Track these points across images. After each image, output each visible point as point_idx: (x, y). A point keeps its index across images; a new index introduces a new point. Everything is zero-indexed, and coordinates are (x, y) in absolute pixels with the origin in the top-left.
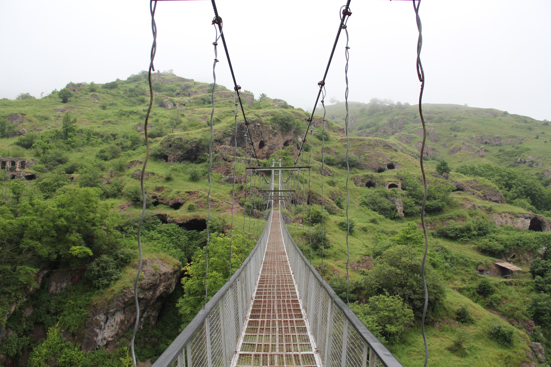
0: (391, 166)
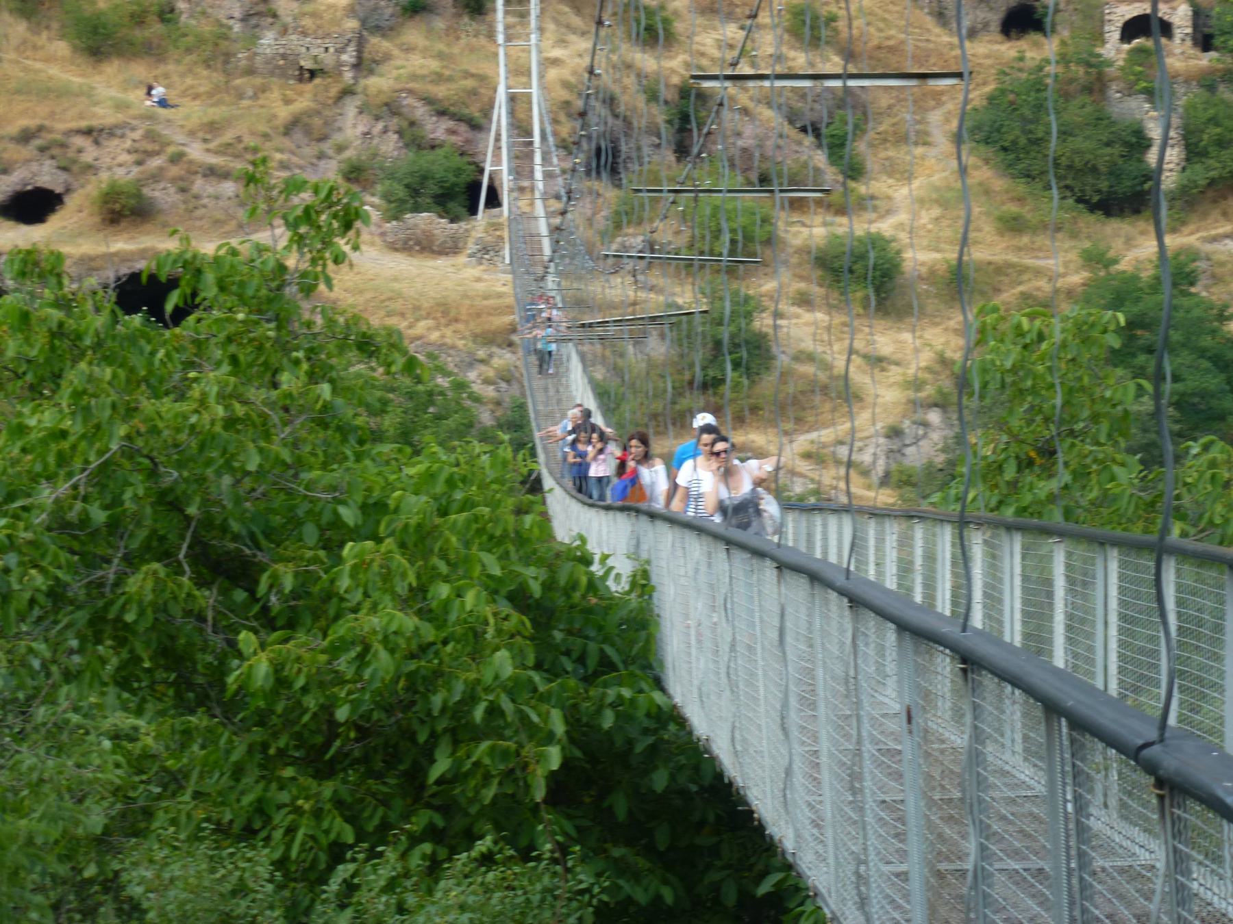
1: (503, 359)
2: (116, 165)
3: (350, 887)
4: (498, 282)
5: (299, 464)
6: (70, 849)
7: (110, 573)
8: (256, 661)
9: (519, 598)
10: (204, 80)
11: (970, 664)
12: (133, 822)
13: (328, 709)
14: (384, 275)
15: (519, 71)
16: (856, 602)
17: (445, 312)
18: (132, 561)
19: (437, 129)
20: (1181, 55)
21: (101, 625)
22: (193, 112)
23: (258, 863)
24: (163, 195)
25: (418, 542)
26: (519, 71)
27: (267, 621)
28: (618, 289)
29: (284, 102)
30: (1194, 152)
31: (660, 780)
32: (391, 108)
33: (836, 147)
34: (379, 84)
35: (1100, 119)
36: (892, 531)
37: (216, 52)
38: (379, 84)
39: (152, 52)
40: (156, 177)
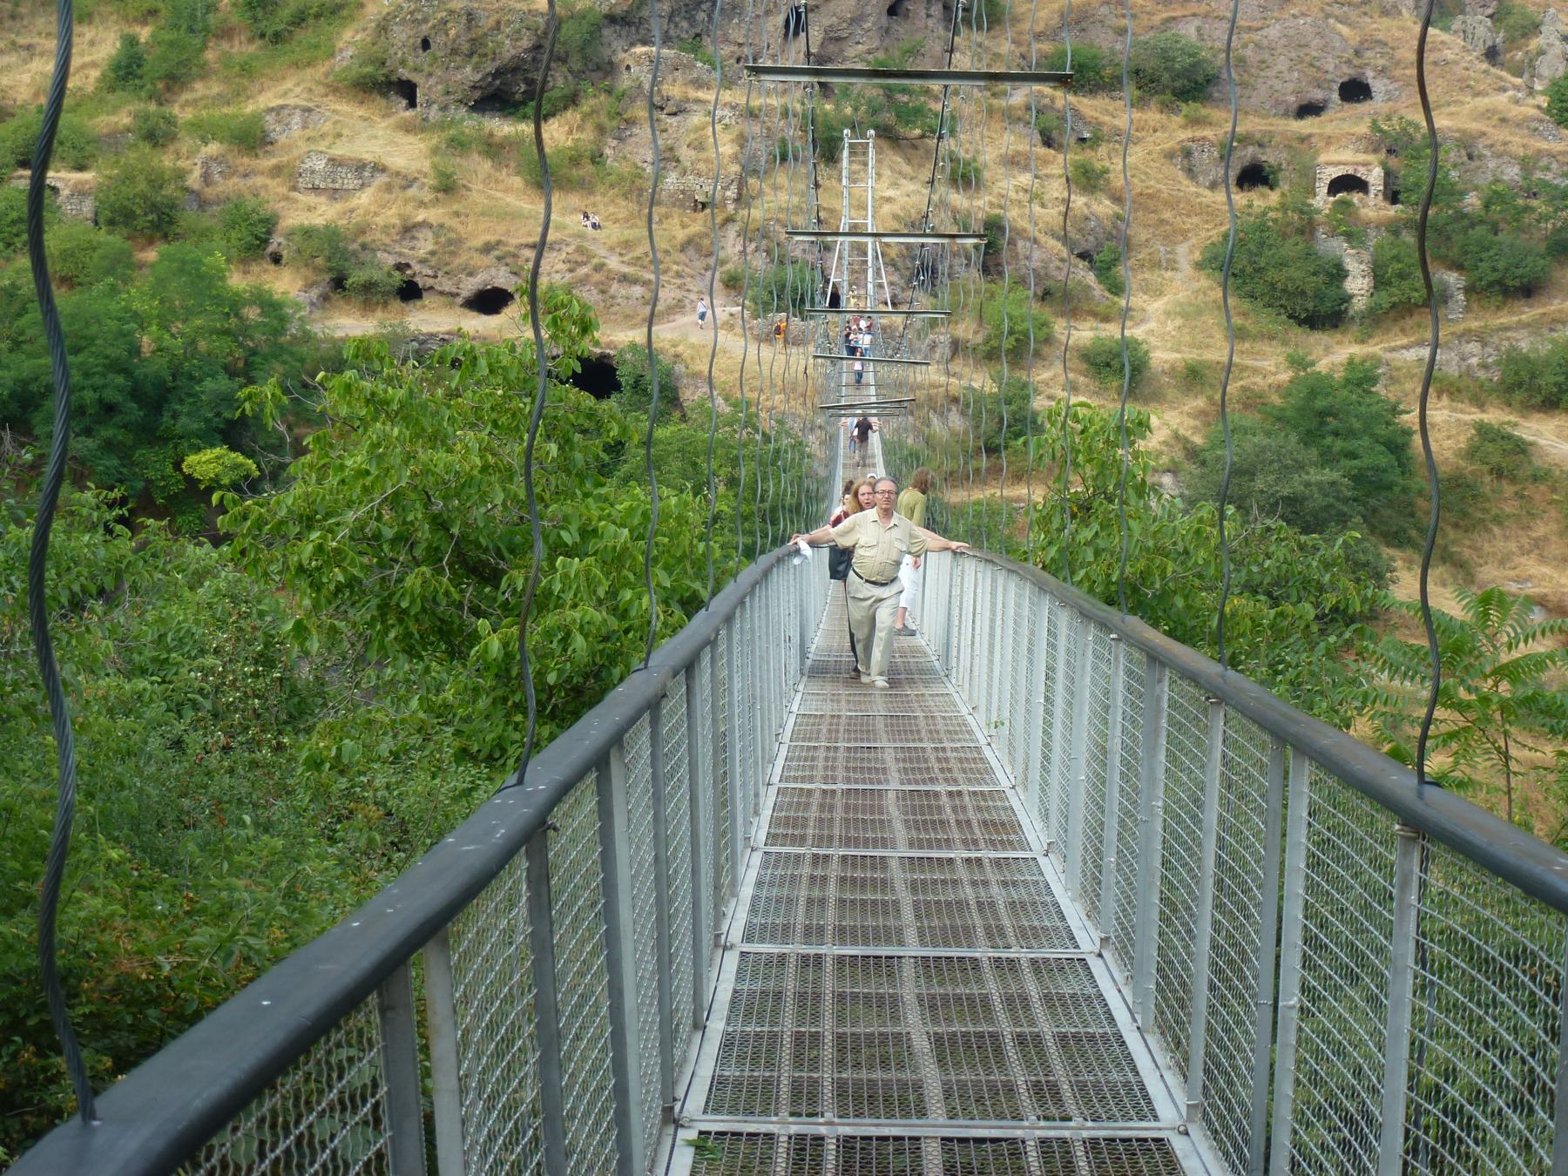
0: (1355, 91)
20: (1372, 207)
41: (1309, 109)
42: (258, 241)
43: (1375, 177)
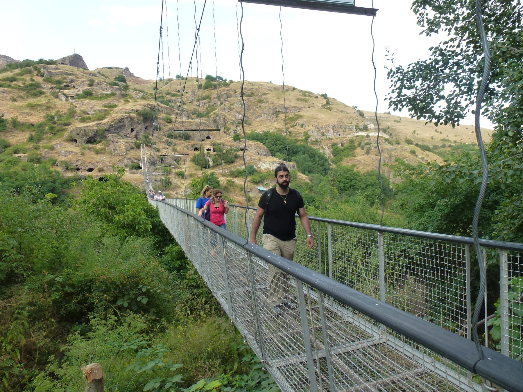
1: (143, 185)
2: (100, 166)
3: (128, 241)
4: (142, 177)
5: (119, 197)
6: (96, 238)
7: (99, 209)
8: (116, 218)
9: (144, 210)
10: (109, 156)
11: (188, 215)
12: (103, 235)
13: (124, 222)
14: (128, 176)
15: (144, 155)
16: (177, 209)
17: (136, 180)
18: (102, 208)
19: (135, 161)
20: (212, 152)
21: (99, 215)
22: (108, 160)
23: (117, 239)
24: (105, 168)
25: (133, 205)
26: (144, 155)
27: (117, 213)
28: (154, 177)
29: (118, 158)
30: (214, 162)
31: (160, 228)
32: (130, 159)
33: (177, 162)
34: (128, 156)
35: (204, 159)
36: (183, 201)
37: (111, 153)
38: (128, 156)
39: (104, 153)
40: (104, 167)
41: (203, 140)
42: (54, 163)
43: (212, 149)
